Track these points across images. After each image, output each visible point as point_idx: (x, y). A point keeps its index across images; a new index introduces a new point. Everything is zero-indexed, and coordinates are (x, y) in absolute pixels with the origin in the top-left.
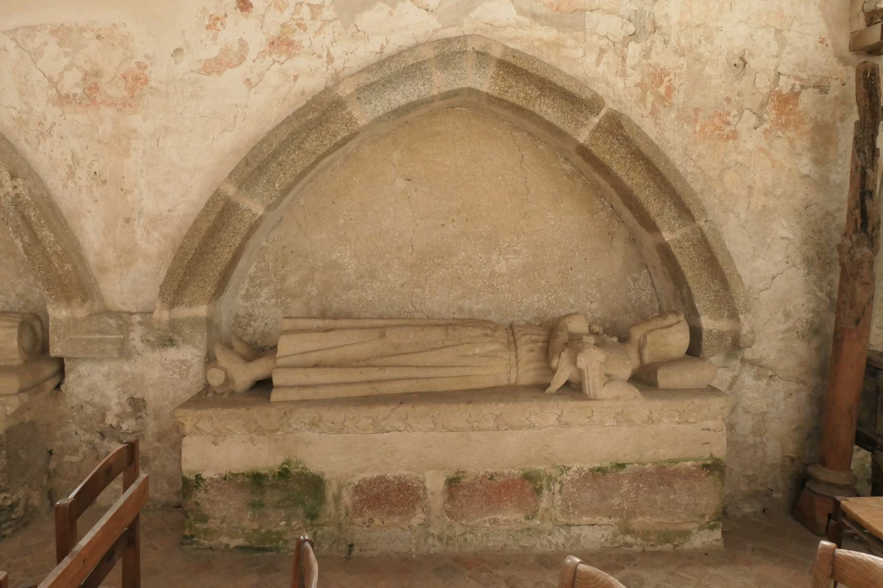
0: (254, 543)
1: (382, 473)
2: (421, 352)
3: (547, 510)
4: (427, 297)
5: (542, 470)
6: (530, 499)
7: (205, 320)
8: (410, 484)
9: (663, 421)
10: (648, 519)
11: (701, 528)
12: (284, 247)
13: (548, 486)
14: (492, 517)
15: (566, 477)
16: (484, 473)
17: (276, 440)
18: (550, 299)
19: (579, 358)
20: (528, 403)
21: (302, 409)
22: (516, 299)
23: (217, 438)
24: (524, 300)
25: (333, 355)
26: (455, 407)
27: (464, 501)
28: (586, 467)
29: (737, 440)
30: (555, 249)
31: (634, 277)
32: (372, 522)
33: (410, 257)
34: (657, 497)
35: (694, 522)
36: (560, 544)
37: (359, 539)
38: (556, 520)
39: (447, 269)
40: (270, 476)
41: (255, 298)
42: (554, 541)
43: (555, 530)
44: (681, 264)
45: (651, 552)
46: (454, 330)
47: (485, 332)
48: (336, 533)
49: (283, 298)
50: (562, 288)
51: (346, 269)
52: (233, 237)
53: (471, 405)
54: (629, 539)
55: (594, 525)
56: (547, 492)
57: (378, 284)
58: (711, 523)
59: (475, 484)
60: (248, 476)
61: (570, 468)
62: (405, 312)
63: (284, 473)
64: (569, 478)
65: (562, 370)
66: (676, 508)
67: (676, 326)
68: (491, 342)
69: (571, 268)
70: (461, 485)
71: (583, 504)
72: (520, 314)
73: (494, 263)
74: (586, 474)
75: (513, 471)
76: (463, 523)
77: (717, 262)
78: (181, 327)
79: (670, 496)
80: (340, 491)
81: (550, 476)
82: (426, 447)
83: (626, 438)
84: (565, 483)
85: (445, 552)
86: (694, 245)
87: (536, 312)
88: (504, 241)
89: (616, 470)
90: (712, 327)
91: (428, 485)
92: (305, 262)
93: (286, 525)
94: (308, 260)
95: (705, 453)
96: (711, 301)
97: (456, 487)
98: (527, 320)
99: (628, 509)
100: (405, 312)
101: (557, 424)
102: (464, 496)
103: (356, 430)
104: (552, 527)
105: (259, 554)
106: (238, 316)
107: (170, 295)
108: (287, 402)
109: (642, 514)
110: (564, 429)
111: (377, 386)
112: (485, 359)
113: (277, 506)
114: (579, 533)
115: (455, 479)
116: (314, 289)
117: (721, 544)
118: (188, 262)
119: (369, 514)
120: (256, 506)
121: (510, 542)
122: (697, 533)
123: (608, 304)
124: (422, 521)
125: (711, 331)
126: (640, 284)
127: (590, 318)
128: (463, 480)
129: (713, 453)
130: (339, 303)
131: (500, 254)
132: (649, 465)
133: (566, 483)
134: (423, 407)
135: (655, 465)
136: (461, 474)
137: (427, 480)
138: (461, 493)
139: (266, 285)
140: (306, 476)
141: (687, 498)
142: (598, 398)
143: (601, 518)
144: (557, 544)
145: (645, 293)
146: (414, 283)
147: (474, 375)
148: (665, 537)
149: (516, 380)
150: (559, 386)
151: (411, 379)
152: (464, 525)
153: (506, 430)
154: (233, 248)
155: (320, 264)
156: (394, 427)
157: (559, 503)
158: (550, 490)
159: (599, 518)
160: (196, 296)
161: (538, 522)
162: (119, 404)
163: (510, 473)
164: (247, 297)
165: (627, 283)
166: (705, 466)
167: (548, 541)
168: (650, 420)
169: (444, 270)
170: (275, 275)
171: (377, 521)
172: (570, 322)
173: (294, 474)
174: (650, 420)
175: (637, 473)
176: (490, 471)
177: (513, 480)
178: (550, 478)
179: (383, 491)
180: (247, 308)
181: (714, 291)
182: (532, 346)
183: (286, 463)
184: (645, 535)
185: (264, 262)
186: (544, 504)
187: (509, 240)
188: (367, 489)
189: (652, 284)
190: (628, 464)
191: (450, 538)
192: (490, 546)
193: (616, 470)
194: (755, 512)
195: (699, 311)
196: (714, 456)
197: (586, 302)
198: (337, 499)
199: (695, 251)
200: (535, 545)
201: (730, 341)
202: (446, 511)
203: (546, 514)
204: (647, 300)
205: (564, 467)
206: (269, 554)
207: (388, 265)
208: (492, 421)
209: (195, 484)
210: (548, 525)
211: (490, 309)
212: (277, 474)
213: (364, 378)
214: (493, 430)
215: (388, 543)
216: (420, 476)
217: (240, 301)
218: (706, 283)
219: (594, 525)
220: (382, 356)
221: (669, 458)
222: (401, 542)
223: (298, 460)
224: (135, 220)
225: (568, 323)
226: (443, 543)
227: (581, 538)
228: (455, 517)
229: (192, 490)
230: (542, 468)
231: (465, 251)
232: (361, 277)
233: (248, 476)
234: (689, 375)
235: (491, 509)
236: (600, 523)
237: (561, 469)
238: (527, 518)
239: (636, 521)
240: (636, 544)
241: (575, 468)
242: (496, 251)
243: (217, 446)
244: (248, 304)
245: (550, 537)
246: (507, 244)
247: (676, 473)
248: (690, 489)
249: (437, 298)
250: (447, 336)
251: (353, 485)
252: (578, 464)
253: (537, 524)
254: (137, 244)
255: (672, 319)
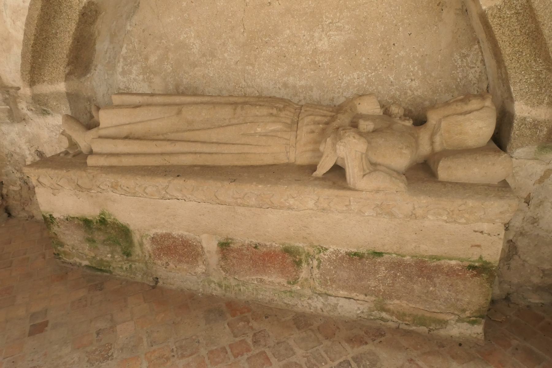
0: (94, 265)
1: (169, 231)
2: (209, 128)
3: (306, 280)
4: (257, 74)
5: (301, 247)
6: (290, 268)
7: (65, 95)
8: (190, 242)
9: (428, 218)
10: (404, 303)
11: (460, 320)
12: (144, 31)
13: (307, 261)
14: (259, 277)
15: (324, 256)
16: (249, 243)
17: (92, 196)
18: (369, 76)
19: (338, 146)
20: (286, 187)
21: (103, 175)
22: (337, 76)
23: (55, 190)
24: (344, 77)
25: (139, 129)
26: (219, 184)
27: (235, 262)
28: (343, 250)
29: (538, 235)
30: (378, 24)
31: (463, 54)
32: (168, 265)
33: (242, 36)
34: (415, 286)
35: (453, 314)
36: (319, 308)
37: (161, 275)
38: (315, 288)
39: (274, 47)
40: (95, 221)
41: (129, 74)
42: (313, 304)
43: (314, 297)
44: (498, 38)
45: (405, 330)
46: (242, 108)
47: (271, 111)
48: (145, 268)
49: (148, 74)
50: (383, 65)
51: (191, 49)
52: (68, 23)
53: (233, 184)
54: (384, 315)
55: (350, 298)
56: (306, 266)
57: (217, 62)
58: (472, 319)
59: (242, 250)
60: (80, 220)
61: (326, 249)
62: (239, 87)
63: (103, 221)
64: (326, 257)
65: (327, 156)
66: (435, 299)
67: (475, 113)
68: (274, 122)
69: (394, 44)
70: (232, 249)
71: (340, 280)
72: (341, 90)
73: (317, 41)
74: (343, 256)
75: (274, 244)
76: (236, 278)
77: (542, 35)
78: (47, 100)
79: (429, 287)
80: (142, 239)
81: (308, 253)
82: (200, 215)
83: (386, 229)
84: (322, 261)
85: (224, 296)
86: (517, 13)
87: (356, 89)
88: (327, 17)
89: (373, 257)
90: (526, 115)
91: (204, 245)
92: (160, 43)
93: (111, 257)
94: (163, 41)
95: (474, 256)
96: (531, 83)
97: (227, 250)
98: (347, 96)
99: (384, 292)
100: (239, 87)
101: (315, 208)
102: (234, 257)
103: (145, 195)
104: (311, 294)
105: (99, 273)
106: (119, 88)
107: (27, 75)
108: (98, 167)
109: (399, 298)
110: (322, 213)
111: (167, 157)
112: (264, 138)
113: (104, 242)
114: (336, 302)
115: (226, 243)
116: (169, 66)
117: (481, 337)
118: (32, 47)
119: (165, 259)
120: (91, 241)
121: (276, 298)
122: (455, 324)
123: (429, 82)
124: (204, 271)
125: (525, 119)
126: (469, 61)
127: (410, 96)
128: (232, 245)
129: (483, 256)
130: (187, 79)
131: (323, 31)
132: (408, 257)
133: (324, 261)
134: (193, 181)
135: (415, 258)
136: (230, 241)
137: (203, 241)
138: (232, 255)
139: (135, 63)
140: (117, 224)
141: (447, 292)
142: (357, 188)
143: (358, 294)
144: (316, 307)
145: (473, 71)
146: (246, 61)
147: (252, 153)
148: (422, 321)
149: (295, 160)
150: (325, 171)
151: (196, 153)
152: (236, 279)
153: (267, 208)
154: (71, 33)
155: (172, 45)
156: (174, 196)
157: (317, 276)
158: (308, 264)
159: (355, 294)
160: (54, 75)
161: (299, 288)
162: (30, 154)
163: (271, 245)
164: (124, 73)
165: (454, 60)
166: (472, 267)
167: (308, 303)
168: (413, 216)
169: (271, 48)
170: (140, 56)
171: (171, 265)
172: (359, 104)
173: (109, 222)
174: (413, 216)
175: (395, 263)
176: (255, 241)
177: (274, 251)
178: (308, 255)
179: (172, 244)
180: (125, 82)
181: (536, 72)
182: (312, 127)
183: (102, 214)
184: (401, 316)
185: (132, 43)
186: (304, 273)
187: (331, 16)
188: (160, 240)
189: (483, 61)
190: (386, 253)
191: (227, 287)
192: (259, 298)
193: (373, 257)
194: (543, 304)
195: (514, 95)
196: (484, 259)
197: (406, 79)
198: (141, 245)
199: (518, 21)
200: (296, 305)
201: (545, 133)
202: (221, 267)
203: (305, 283)
204: (474, 79)
205: (322, 247)
206: (105, 274)
207: (224, 44)
208: (254, 200)
209: (50, 221)
210: (308, 292)
211: (312, 85)
212: (98, 221)
213: (159, 150)
214: (256, 207)
215: (182, 282)
216: (197, 237)
217: (120, 77)
218: (528, 62)
219: (350, 298)
220: (177, 131)
221: (431, 254)
222: (191, 282)
223: (110, 213)
224: (3, 12)
225: (358, 105)
226: (222, 289)
227: (338, 307)
228: (229, 272)
229: (50, 224)
230: (301, 245)
231: (289, 28)
232: (204, 55)
233: (80, 220)
234: (476, 170)
235: (257, 271)
236: (357, 298)
237: (318, 249)
238: (289, 283)
239: (392, 303)
240: (392, 322)
241: (332, 250)
242: (319, 28)
243: (56, 196)
244: (125, 80)
245: (310, 301)
246: (330, 21)
247: (438, 269)
248: (451, 285)
249: (265, 75)
250: (235, 114)
251: (150, 237)
252: (335, 246)
253: (297, 289)
254: (10, 33)
255: (474, 104)
